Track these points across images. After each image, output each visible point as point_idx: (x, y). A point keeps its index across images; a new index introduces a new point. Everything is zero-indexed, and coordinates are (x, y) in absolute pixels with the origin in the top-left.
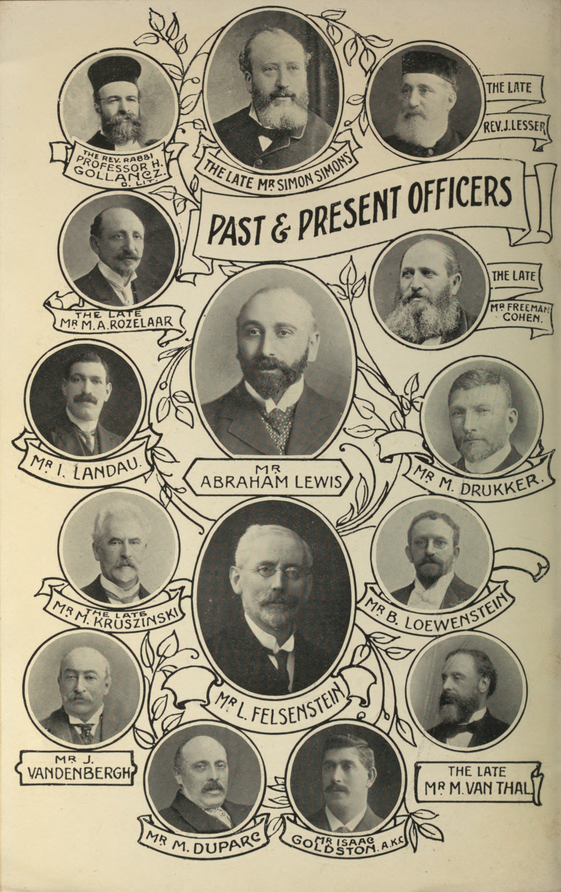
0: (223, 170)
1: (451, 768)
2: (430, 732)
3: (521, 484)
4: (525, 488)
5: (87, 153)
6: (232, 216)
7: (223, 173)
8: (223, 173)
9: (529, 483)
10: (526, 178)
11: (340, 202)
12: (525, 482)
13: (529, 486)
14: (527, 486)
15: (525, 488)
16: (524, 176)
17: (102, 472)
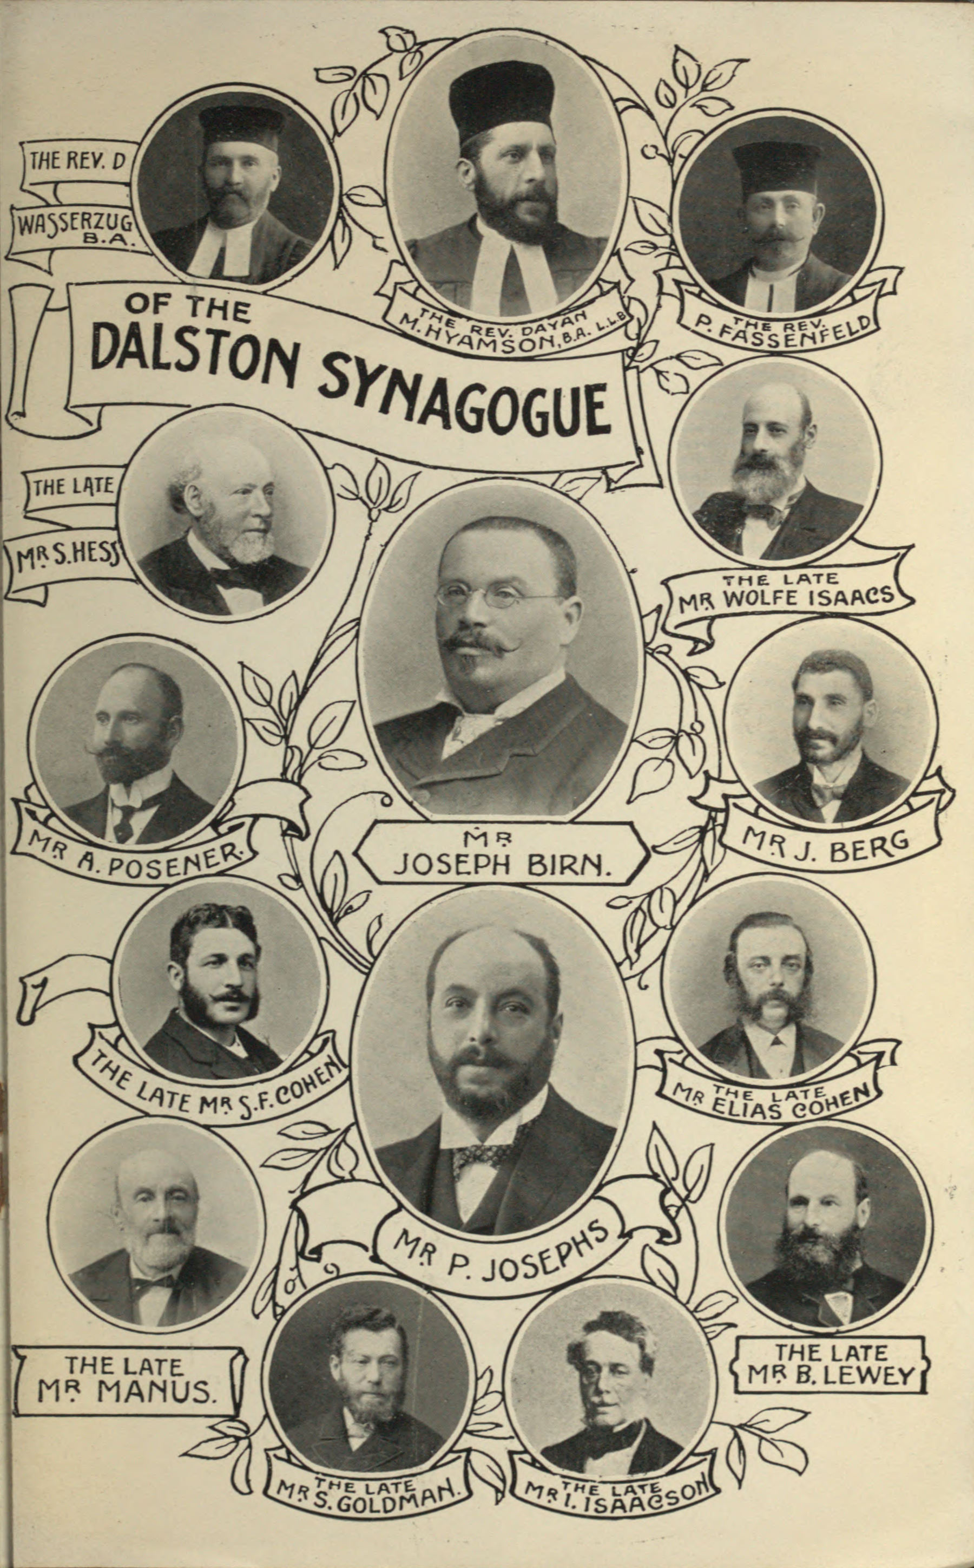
0: (598, 397)
1: (781, 1346)
2: (750, 1287)
3: (862, 849)
4: (866, 858)
5: (203, 307)
6: (442, 376)
7: (600, 405)
8: (600, 405)
9: (874, 849)
10: (66, 304)
11: (605, 385)
12: (867, 846)
13: (874, 855)
14: (869, 854)
15: (866, 858)
16: (69, 307)
17: (163, 1390)
